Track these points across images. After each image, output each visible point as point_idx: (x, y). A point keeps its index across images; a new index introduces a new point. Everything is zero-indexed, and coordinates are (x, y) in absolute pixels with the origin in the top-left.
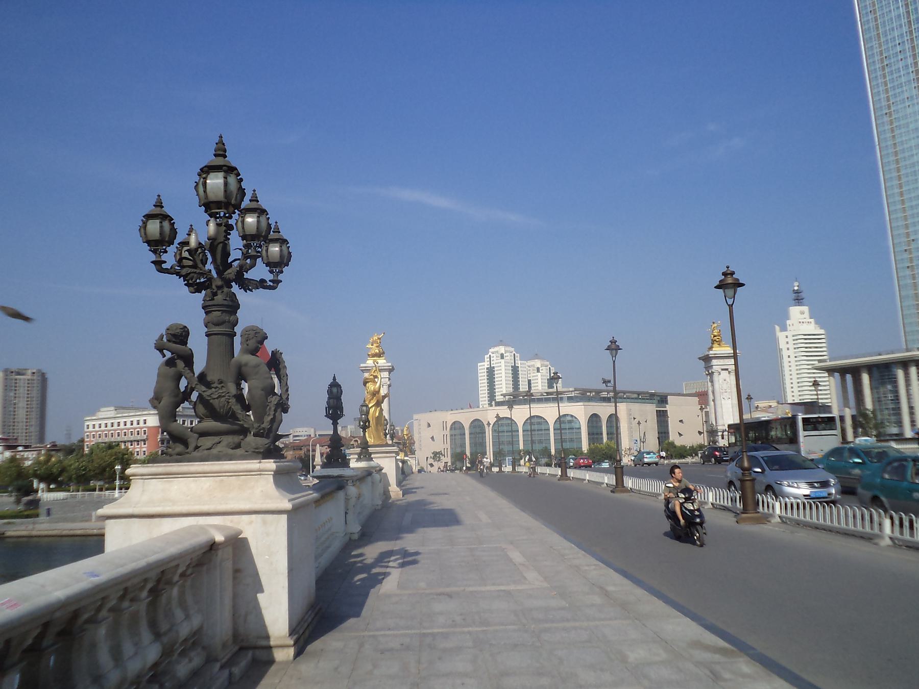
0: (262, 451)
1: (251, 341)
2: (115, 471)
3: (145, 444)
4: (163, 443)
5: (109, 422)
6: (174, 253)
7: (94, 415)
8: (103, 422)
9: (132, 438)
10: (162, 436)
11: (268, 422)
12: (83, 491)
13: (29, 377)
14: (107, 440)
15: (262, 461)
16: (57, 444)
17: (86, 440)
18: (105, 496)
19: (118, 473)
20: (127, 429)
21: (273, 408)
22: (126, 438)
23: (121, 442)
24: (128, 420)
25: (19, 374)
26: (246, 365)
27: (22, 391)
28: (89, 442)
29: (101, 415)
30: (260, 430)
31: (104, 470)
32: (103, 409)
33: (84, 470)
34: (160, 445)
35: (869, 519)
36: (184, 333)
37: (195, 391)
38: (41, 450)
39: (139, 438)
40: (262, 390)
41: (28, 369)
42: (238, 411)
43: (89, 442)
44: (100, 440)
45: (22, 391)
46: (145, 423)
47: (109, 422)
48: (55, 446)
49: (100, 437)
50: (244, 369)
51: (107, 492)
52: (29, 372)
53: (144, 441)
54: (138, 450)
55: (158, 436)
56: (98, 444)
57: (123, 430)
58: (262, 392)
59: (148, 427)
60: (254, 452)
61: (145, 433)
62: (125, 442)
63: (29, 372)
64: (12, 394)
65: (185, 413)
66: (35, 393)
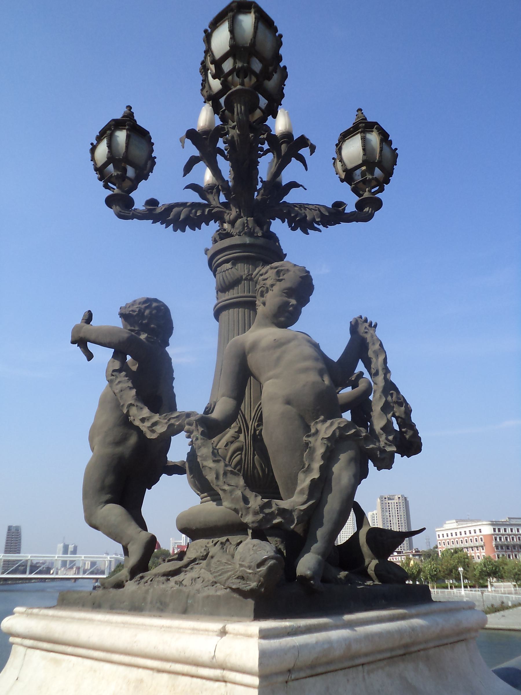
0: (253, 585)
1: (270, 292)
2: (459, 572)
3: (483, 549)
4: (497, 549)
5: (454, 532)
6: (91, 147)
7: (442, 526)
8: (449, 533)
9: (472, 545)
10: (495, 542)
11: (302, 492)
12: (437, 588)
13: (397, 501)
14: (454, 546)
15: (231, 627)
16: (419, 550)
17: (439, 546)
18: (454, 594)
19: (461, 574)
20: (472, 537)
21: (320, 450)
22: (467, 545)
23: (465, 548)
24: (467, 530)
25: (389, 499)
26: (254, 346)
27: (394, 512)
28: (441, 549)
29: (446, 526)
30: (272, 516)
31: (451, 571)
32: (447, 522)
33: (435, 571)
34: (496, 550)
35: (515, 520)
36: (147, 312)
37: (183, 431)
38: (409, 555)
39: (477, 544)
40: (288, 402)
41: (396, 495)
42: (205, 463)
43: (441, 549)
44: (449, 547)
45: (394, 512)
46: (480, 532)
47: (454, 532)
48: (418, 551)
49: (449, 544)
50: (252, 361)
51: (455, 590)
52: (396, 497)
53: (482, 547)
54: (478, 554)
55: (492, 542)
56: (448, 550)
57: (469, 537)
58: (289, 407)
59: (484, 536)
60: (237, 591)
61: (482, 540)
62: (467, 548)
63: (396, 497)
64: (388, 514)
65: (512, 523)
66: (402, 513)
